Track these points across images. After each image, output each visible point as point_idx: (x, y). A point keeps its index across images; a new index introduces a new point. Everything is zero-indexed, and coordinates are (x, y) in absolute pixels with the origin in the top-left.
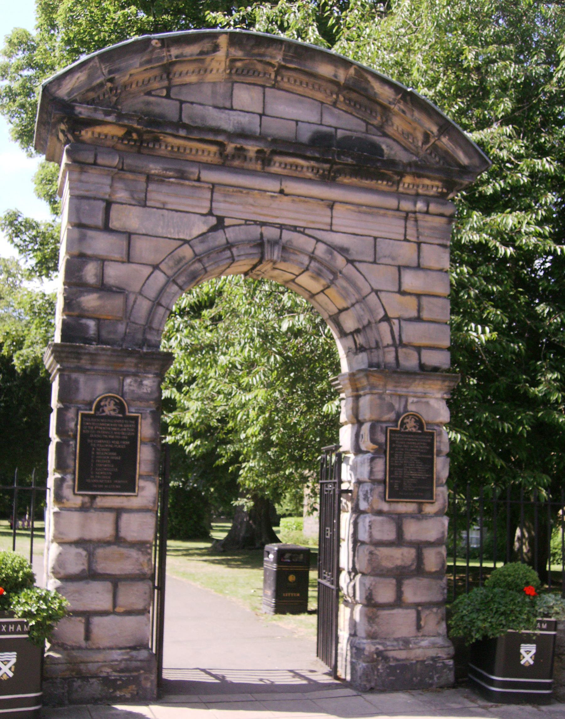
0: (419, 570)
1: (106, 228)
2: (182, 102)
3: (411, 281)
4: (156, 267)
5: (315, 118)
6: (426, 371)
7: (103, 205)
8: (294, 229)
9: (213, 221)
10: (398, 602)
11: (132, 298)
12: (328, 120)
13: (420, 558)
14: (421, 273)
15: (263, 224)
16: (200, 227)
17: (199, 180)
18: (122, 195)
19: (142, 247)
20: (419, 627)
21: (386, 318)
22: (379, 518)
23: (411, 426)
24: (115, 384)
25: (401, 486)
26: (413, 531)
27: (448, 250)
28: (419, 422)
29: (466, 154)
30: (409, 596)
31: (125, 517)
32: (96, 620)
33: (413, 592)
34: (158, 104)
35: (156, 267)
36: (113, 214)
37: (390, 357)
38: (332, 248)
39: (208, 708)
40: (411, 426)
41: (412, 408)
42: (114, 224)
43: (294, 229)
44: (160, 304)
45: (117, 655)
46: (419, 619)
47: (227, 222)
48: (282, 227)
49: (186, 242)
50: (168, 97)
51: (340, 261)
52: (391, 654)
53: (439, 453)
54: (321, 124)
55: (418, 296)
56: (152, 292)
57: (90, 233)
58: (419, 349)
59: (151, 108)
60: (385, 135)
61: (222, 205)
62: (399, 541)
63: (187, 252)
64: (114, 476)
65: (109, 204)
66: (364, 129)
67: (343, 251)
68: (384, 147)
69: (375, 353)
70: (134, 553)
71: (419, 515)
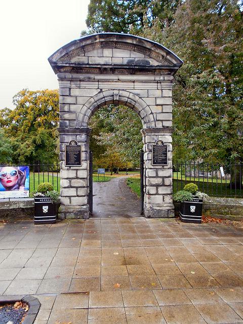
0: (163, 185)
1: (70, 95)
2: (88, 57)
3: (159, 101)
4: (84, 105)
5: (128, 56)
6: (165, 128)
7: (68, 89)
8: (123, 90)
9: (99, 90)
10: (157, 194)
11: (78, 114)
12: (132, 56)
13: (163, 181)
14: (163, 99)
15: (114, 89)
16: (96, 92)
17: (94, 79)
18: (73, 86)
19: (80, 100)
20: (164, 201)
21: (152, 113)
22: (151, 170)
23: (160, 144)
24: (74, 137)
25: (157, 161)
26: (161, 173)
27: (171, 91)
28: (162, 142)
29: (176, 60)
30: (160, 192)
31: (79, 172)
32: (72, 198)
33: (161, 190)
34: (81, 59)
35: (84, 105)
36: (71, 92)
37: (153, 125)
38: (134, 94)
39: (72, 42)
40: (160, 144)
41: (160, 139)
42: (72, 94)
43: (123, 90)
44: (85, 115)
45: (78, 207)
46: (163, 198)
47: (103, 90)
48: (119, 90)
49: (92, 97)
50: (84, 56)
51: (137, 98)
52: (154, 208)
53: (169, 151)
54: (77, 170)
55: (162, 105)
56: (83, 112)
57: (65, 97)
58: (162, 121)
59: (80, 60)
60: (151, 58)
61: (101, 86)
62: (157, 176)
63: (92, 100)
64: (75, 161)
65: (70, 89)
66: (144, 57)
67: (138, 95)
68: (150, 61)
69: (148, 124)
70: (81, 181)
71: (163, 169)
